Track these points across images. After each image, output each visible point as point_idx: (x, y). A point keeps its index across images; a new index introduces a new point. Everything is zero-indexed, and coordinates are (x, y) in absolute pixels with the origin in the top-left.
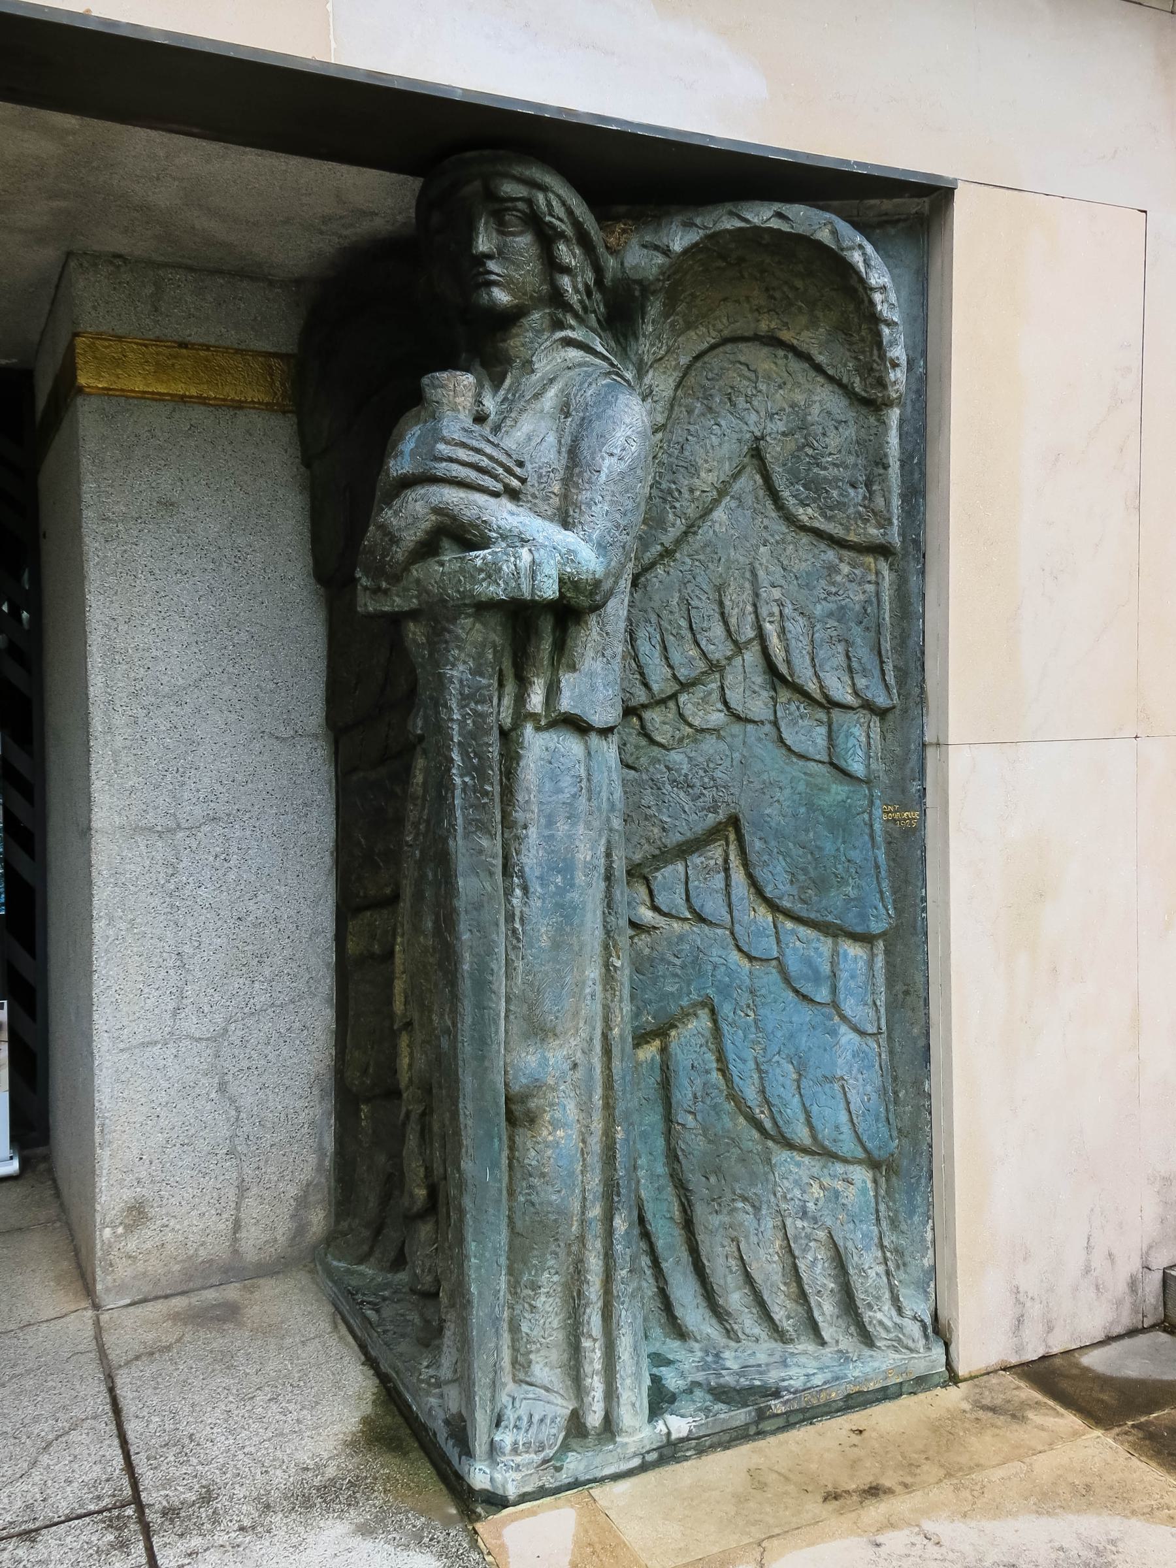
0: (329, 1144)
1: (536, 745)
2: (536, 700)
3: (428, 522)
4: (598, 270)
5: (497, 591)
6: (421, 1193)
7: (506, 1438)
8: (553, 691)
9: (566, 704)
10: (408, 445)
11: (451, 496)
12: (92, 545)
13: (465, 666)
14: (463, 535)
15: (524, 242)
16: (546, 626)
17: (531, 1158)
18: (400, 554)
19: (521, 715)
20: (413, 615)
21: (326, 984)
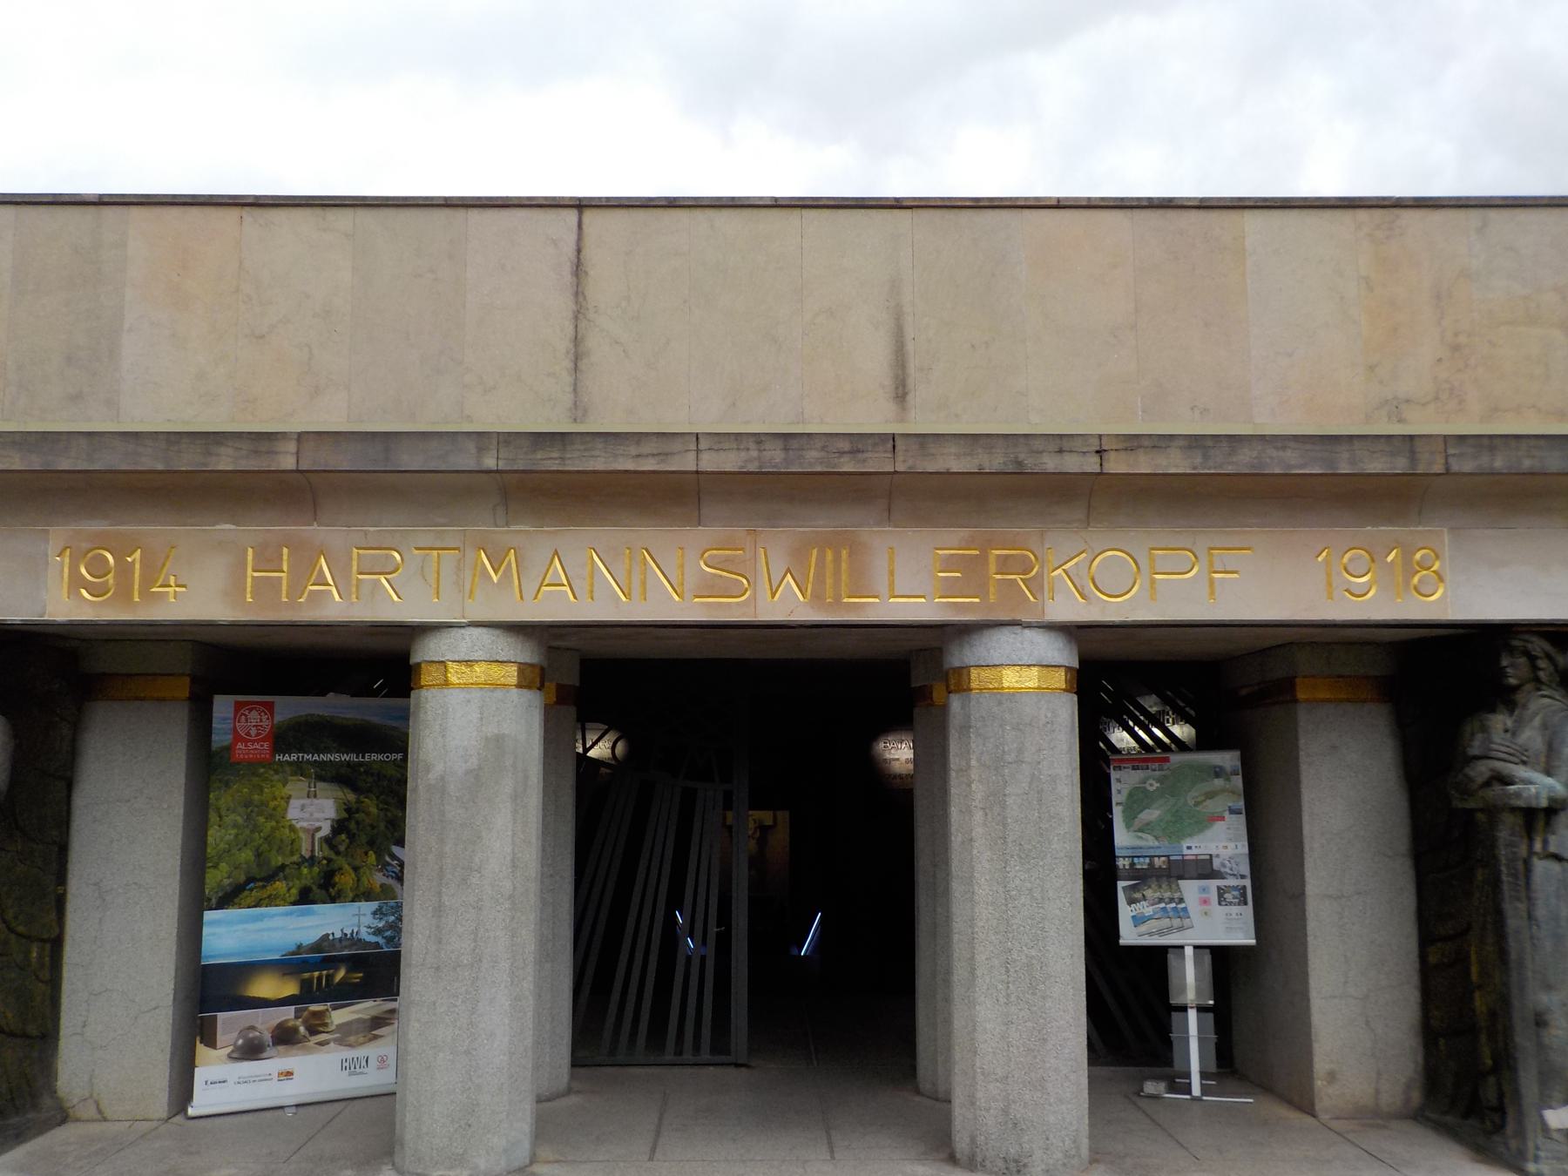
0: (1420, 1059)
1: (1541, 867)
2: (1538, 846)
3: (1487, 774)
4: (1555, 665)
5: (1521, 803)
6: (1489, 1062)
7: (1542, 1154)
8: (1545, 842)
9: (1552, 849)
10: (1476, 743)
11: (1498, 765)
12: (1303, 767)
13: (1506, 831)
14: (1505, 780)
15: (1523, 660)
16: (1542, 816)
17: (1546, 1041)
18: (1475, 786)
19: (1531, 853)
20: (1481, 810)
21: (1415, 979)
